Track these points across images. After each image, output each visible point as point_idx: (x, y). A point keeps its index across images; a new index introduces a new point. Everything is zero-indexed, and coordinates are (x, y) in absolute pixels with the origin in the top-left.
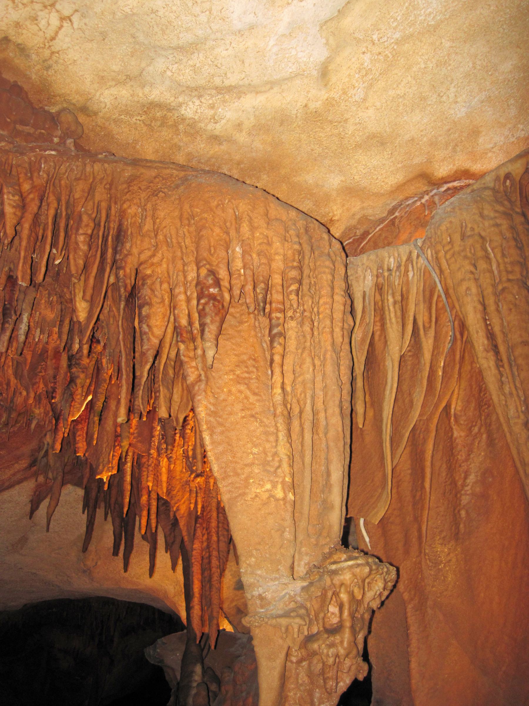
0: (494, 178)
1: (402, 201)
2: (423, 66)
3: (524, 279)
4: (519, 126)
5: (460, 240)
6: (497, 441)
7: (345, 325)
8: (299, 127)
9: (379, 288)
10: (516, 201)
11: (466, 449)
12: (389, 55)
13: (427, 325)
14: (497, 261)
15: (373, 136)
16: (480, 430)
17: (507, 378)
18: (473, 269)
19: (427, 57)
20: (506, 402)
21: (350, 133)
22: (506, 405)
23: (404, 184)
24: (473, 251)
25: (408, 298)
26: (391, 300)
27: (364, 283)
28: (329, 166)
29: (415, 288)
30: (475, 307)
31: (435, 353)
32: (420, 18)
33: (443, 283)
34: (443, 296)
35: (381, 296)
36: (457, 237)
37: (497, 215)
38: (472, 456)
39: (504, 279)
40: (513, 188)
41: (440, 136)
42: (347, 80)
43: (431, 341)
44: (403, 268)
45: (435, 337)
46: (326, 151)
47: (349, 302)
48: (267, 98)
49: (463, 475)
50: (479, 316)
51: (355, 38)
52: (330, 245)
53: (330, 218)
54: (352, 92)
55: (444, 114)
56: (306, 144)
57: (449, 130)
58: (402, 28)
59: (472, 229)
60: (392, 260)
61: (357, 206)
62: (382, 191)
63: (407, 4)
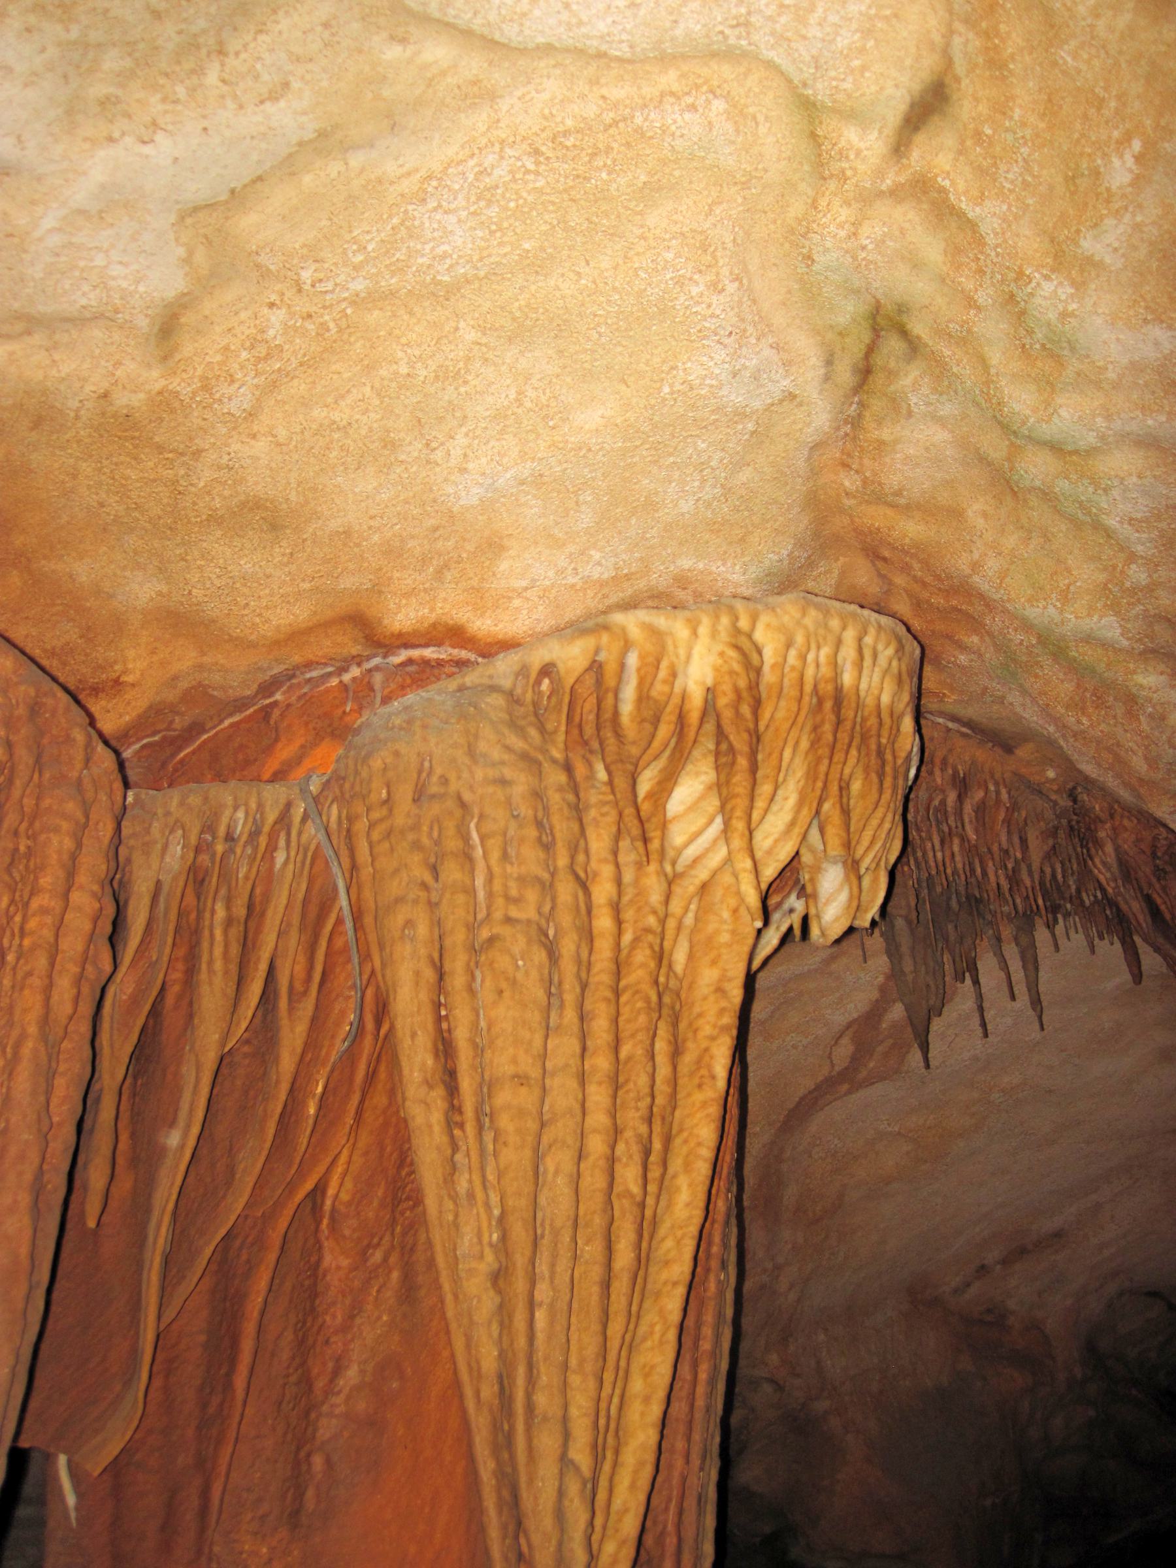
0: (516, 668)
1: (296, 667)
2: (404, 370)
3: (543, 922)
4: (593, 552)
5: (410, 798)
6: (423, 1292)
7: (89, 968)
8: (79, 442)
9: (196, 878)
10: (555, 732)
11: (348, 1301)
12: (332, 325)
13: (299, 987)
14: (489, 868)
15: (255, 505)
16: (385, 1259)
17: (468, 1155)
18: (428, 877)
19: (417, 353)
20: (456, 1216)
21: (202, 484)
22: (456, 1225)
23: (309, 630)
24: (435, 834)
25: (263, 914)
26: (221, 913)
27: (161, 862)
28: (136, 553)
29: (285, 893)
30: (417, 974)
31: (308, 1059)
32: (420, 261)
33: (354, 898)
34: (349, 924)
35: (199, 899)
36: (404, 793)
37: (506, 757)
38: (358, 1321)
39: (498, 915)
40: (554, 700)
41: (413, 537)
42: (219, 358)
43: (301, 1028)
44: (263, 841)
45: (314, 1019)
46: (136, 514)
47: (110, 911)
48: (12, 353)
49: (330, 1365)
50: (424, 996)
51: (258, 266)
52: (87, 761)
53: (114, 675)
54: (225, 390)
55: (431, 490)
56: (89, 487)
57: (436, 529)
58: (374, 270)
59: (444, 781)
60: (240, 815)
61: (185, 659)
62: (253, 637)
63: (395, 221)
